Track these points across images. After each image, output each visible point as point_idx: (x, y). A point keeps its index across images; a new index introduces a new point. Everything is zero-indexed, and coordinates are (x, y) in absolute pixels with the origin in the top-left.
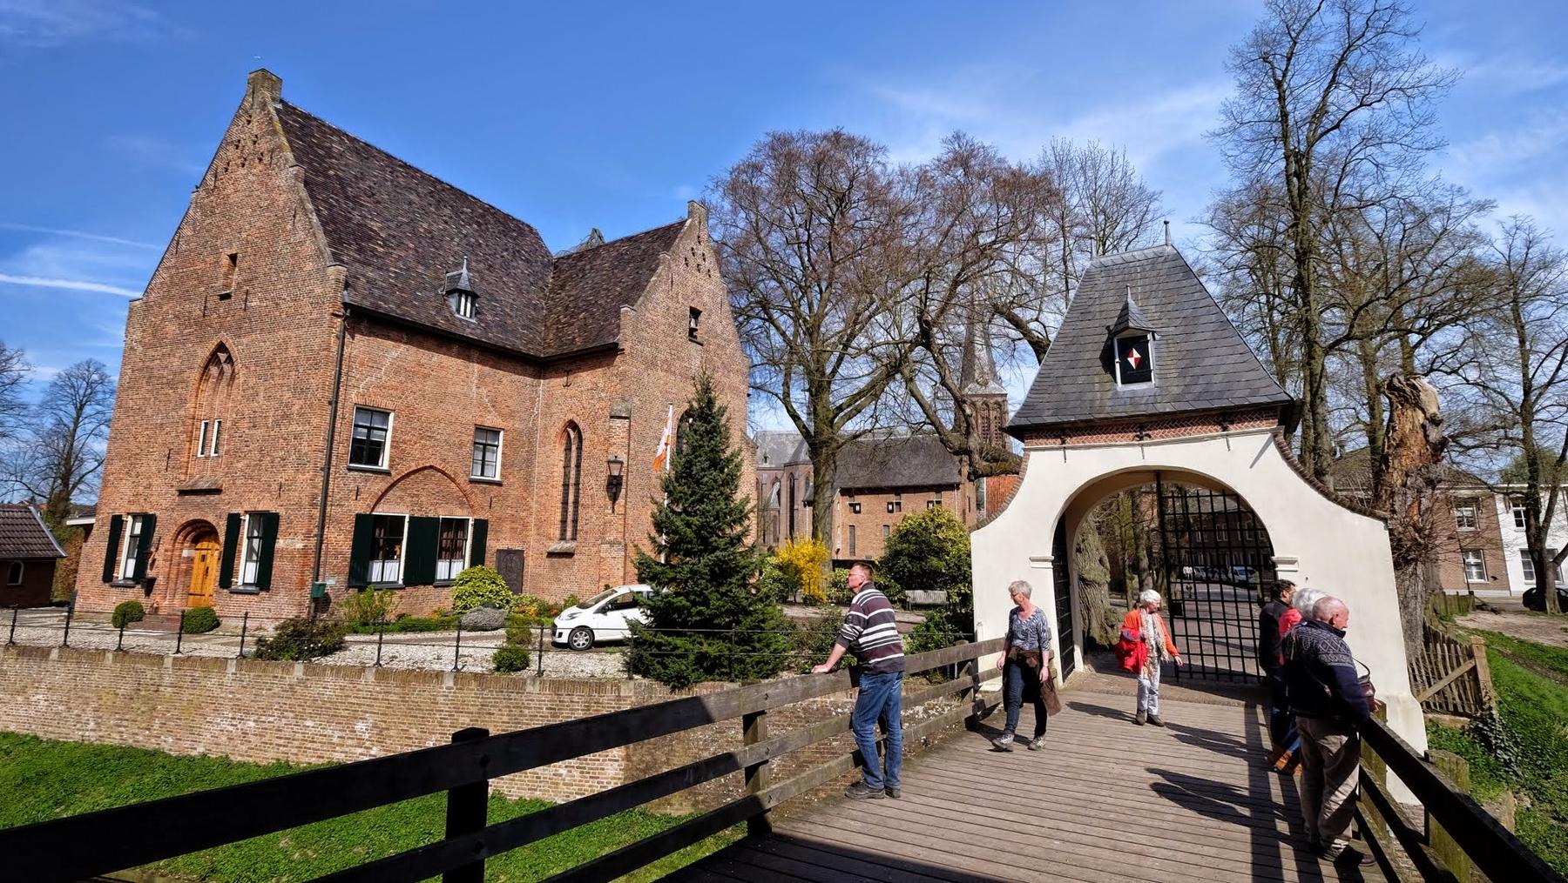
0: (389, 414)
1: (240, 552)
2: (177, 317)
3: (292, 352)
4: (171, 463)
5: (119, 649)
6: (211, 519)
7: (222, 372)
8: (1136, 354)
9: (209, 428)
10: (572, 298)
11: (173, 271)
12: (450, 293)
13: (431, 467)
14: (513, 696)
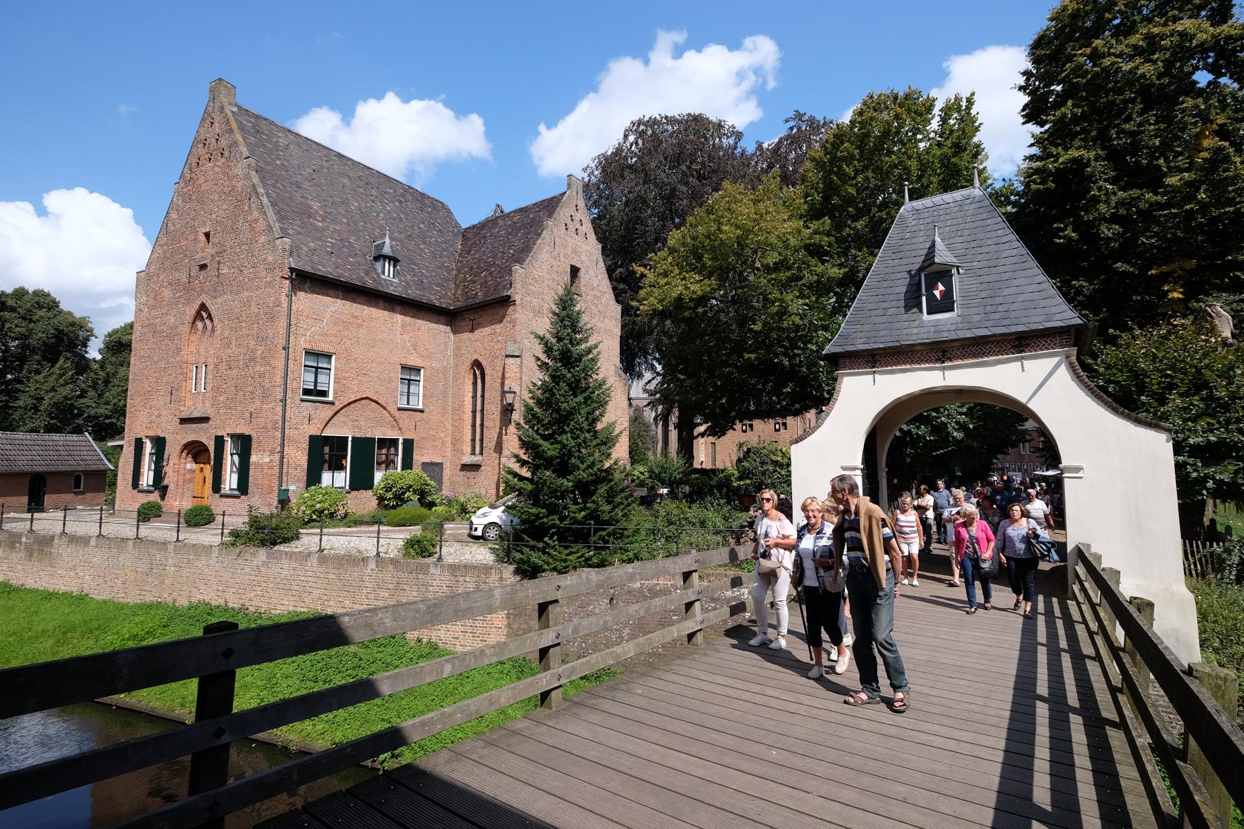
0: (331, 356)
1: (226, 465)
2: (170, 284)
3: (254, 309)
4: (174, 398)
5: (138, 538)
7: (205, 327)
8: (941, 287)
9: (199, 370)
10: (476, 260)
11: (165, 248)
12: (376, 259)
13: (367, 398)
14: (420, 576)
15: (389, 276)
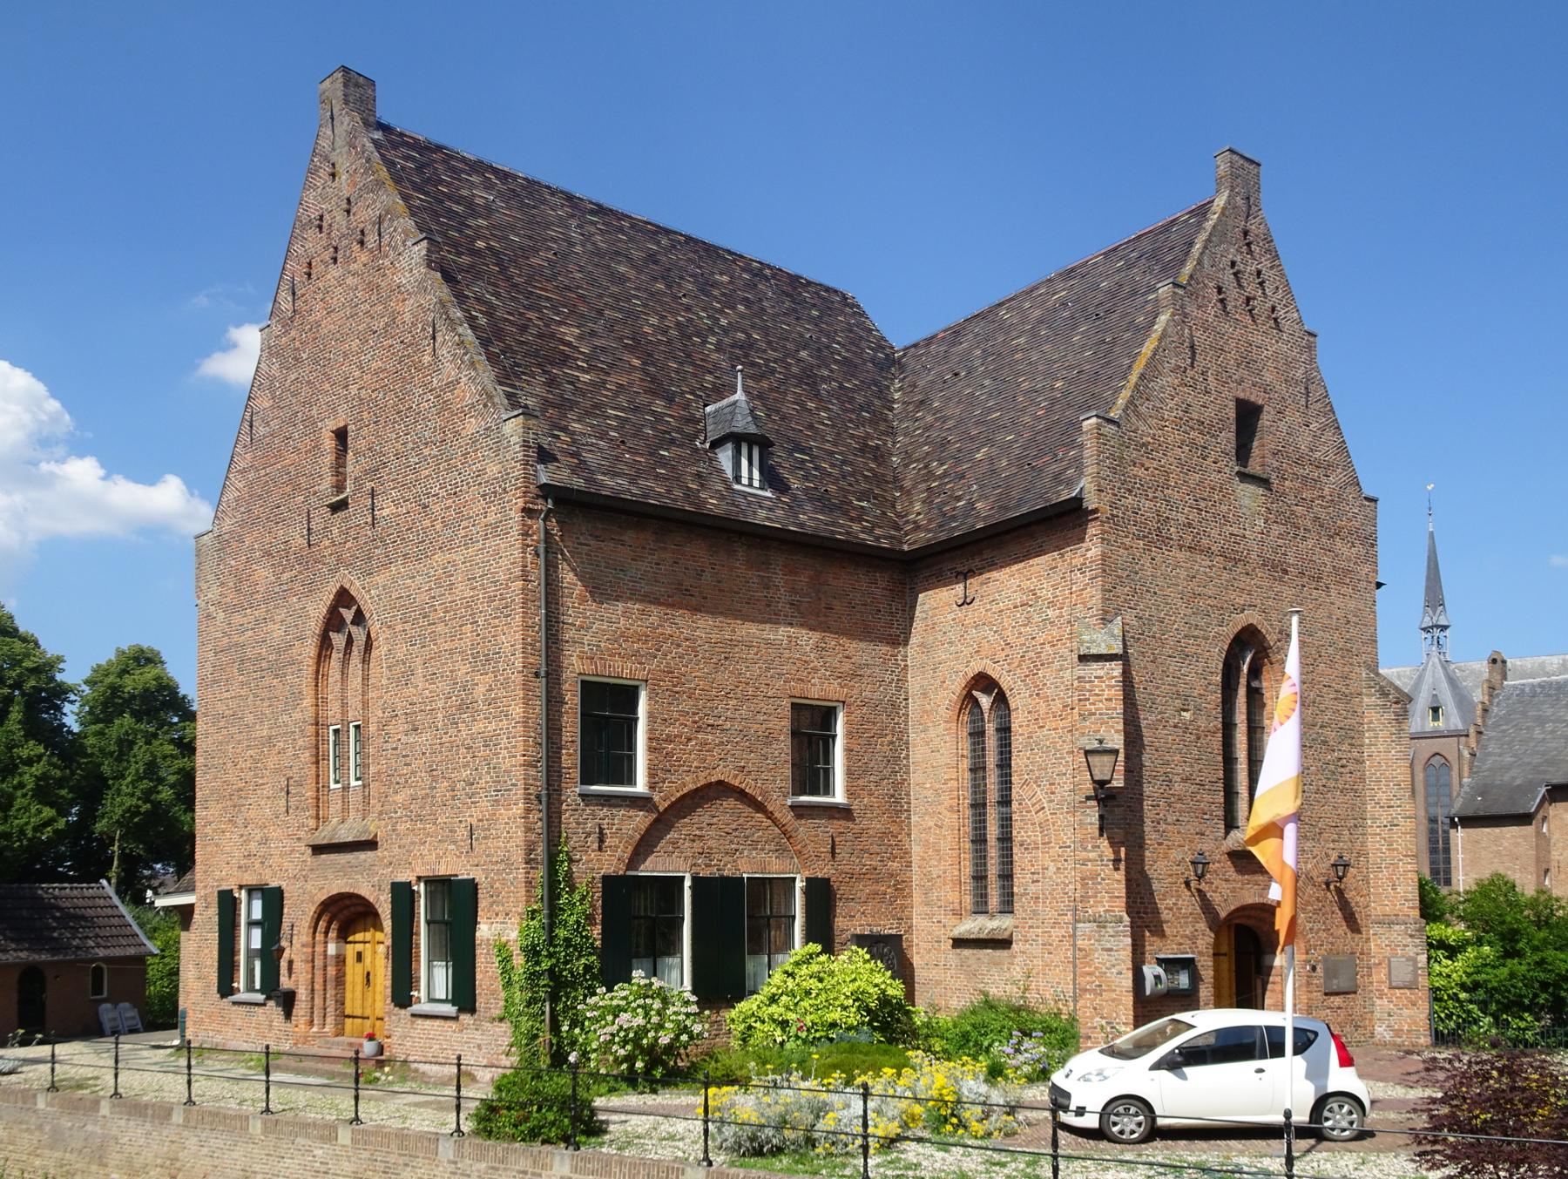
2: (268, 554)
3: (463, 590)
6: (365, 891)
10: (951, 423)
15: (750, 485)
